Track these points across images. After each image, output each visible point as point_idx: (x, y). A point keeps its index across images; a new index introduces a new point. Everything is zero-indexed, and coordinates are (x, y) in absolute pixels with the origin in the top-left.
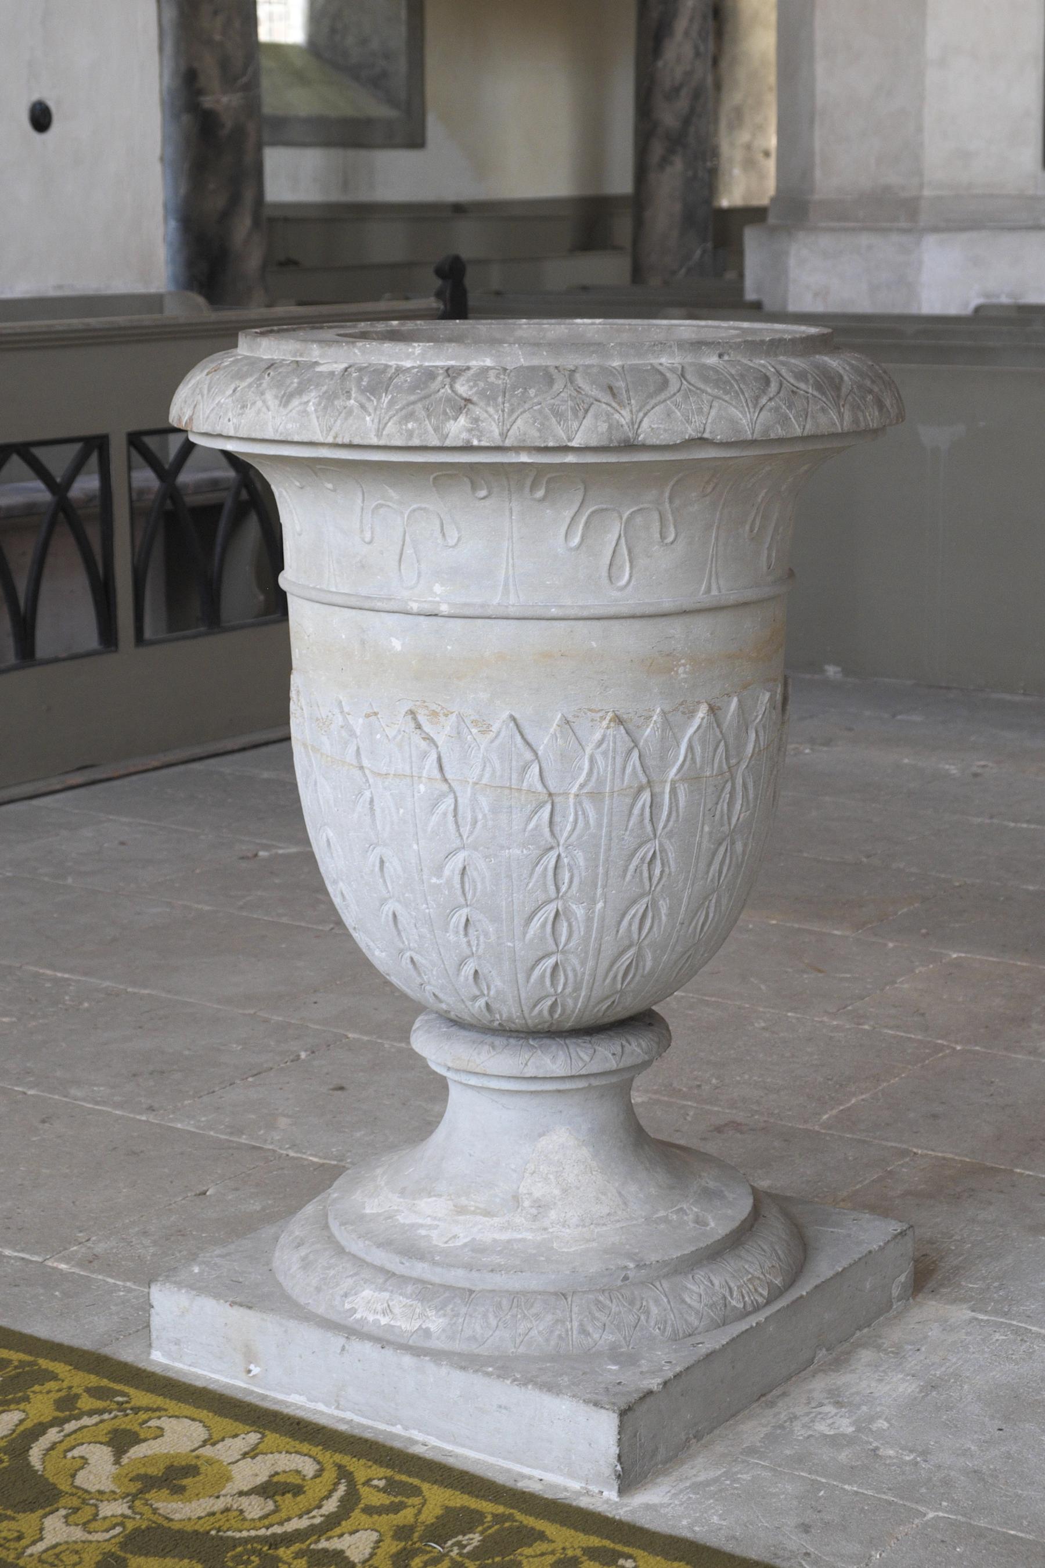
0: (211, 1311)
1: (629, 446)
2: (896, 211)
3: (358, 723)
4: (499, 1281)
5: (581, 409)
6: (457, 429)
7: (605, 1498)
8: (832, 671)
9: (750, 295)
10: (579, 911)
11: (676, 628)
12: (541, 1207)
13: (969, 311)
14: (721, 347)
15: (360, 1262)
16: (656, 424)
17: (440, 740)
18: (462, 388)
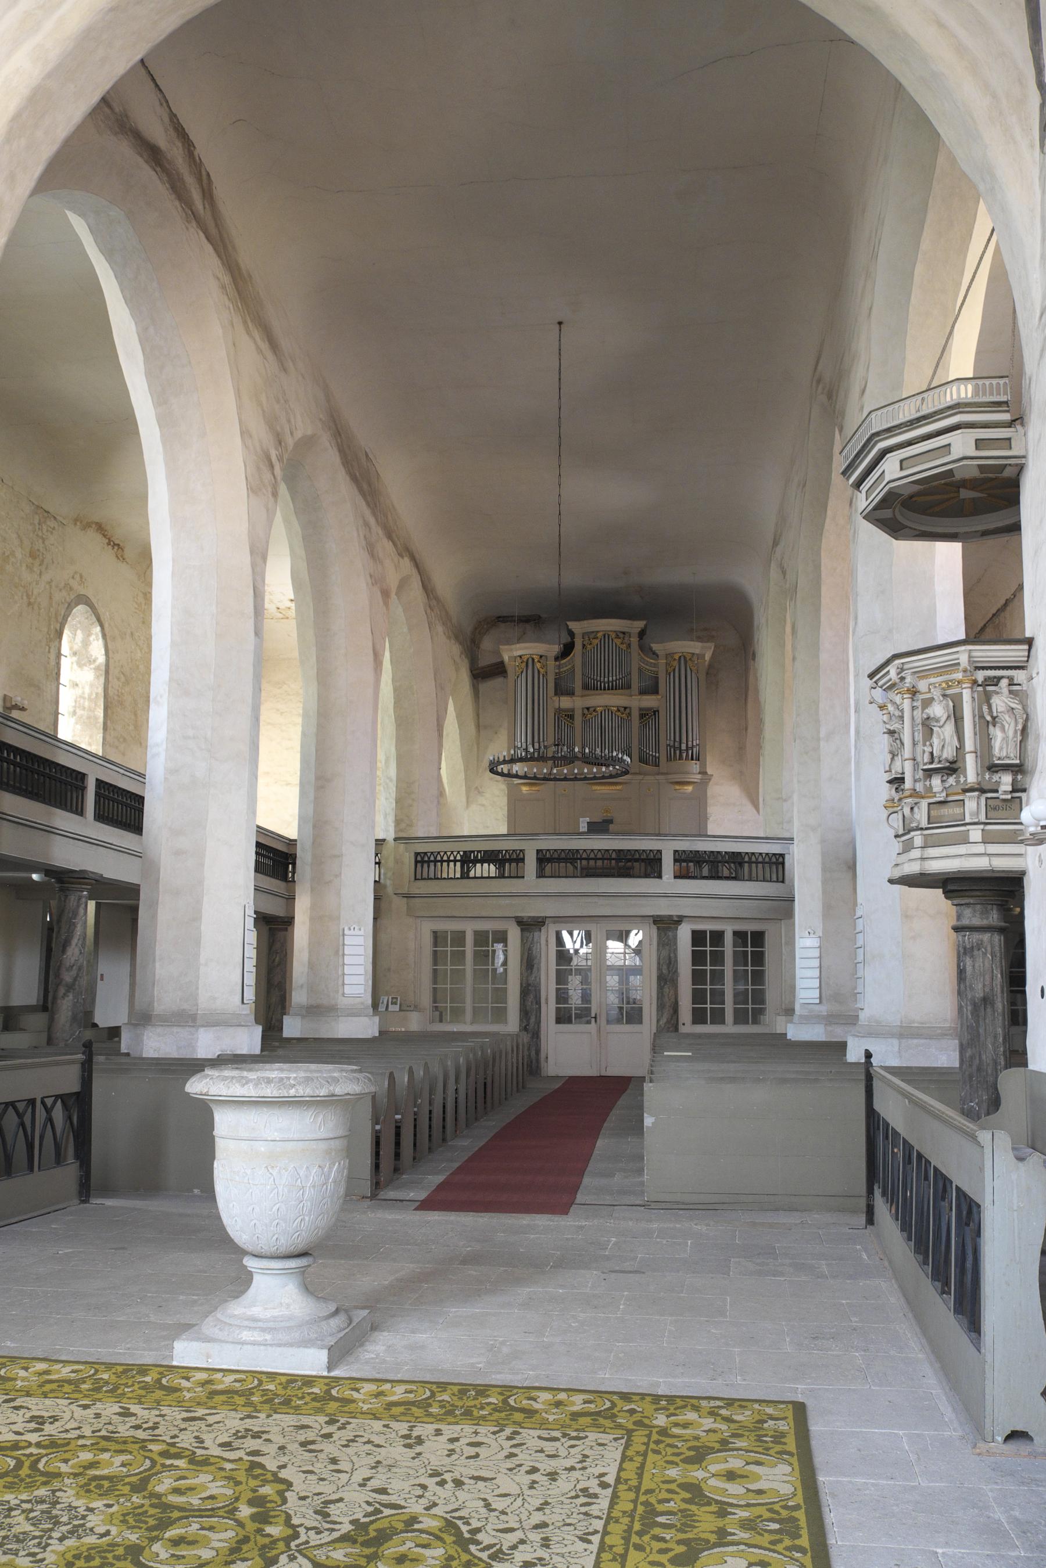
0: (195, 1345)
1: (333, 1095)
2: (187, 1019)
3: (249, 1172)
4: (283, 1324)
5: (322, 1086)
6: (292, 1092)
7: (325, 1374)
8: (196, 1191)
9: (124, 1050)
10: (307, 1218)
11: (332, 1142)
12: (288, 1305)
13: (215, 1057)
14: (346, 1071)
15: (240, 1327)
16: (339, 1090)
17: (274, 1174)
18: (292, 1082)
